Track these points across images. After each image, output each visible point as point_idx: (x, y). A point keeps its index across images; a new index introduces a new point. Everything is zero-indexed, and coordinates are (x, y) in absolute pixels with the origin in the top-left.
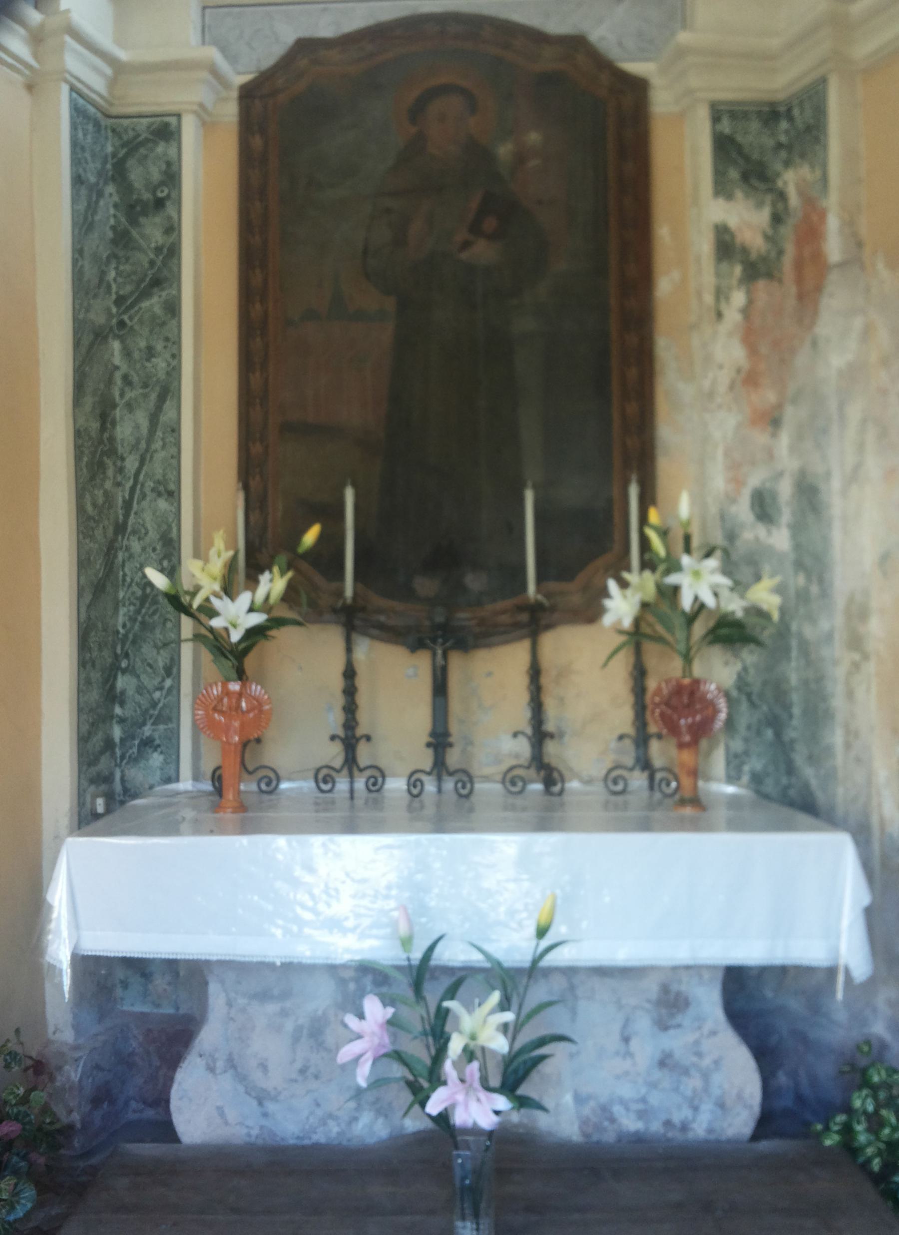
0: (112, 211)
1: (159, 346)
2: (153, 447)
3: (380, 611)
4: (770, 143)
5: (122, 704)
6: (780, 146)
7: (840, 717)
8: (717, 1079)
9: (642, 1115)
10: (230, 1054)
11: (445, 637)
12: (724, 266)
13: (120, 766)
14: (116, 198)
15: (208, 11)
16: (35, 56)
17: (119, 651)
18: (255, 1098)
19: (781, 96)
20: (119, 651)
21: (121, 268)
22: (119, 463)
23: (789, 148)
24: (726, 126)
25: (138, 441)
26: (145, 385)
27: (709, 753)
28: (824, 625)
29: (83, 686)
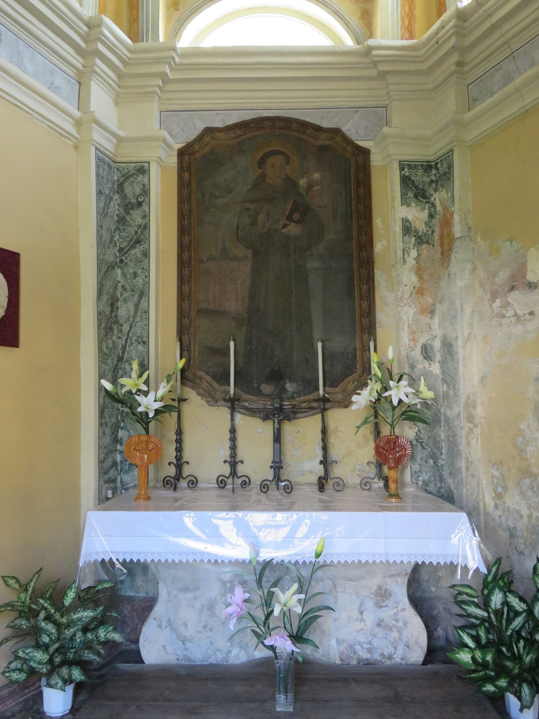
0: (117, 207)
1: (139, 272)
2: (136, 320)
3: (245, 401)
4: (428, 180)
5: (121, 444)
6: (432, 181)
7: (463, 454)
8: (405, 633)
9: (369, 650)
10: (169, 618)
11: (280, 414)
12: (407, 237)
13: (120, 475)
14: (119, 201)
15: (162, 113)
16: (78, 132)
17: (119, 418)
18: (181, 641)
19: (432, 158)
20: (119, 418)
21: (121, 234)
22: (120, 328)
23: (436, 182)
24: (406, 172)
25: (129, 317)
26: (133, 291)
27: (403, 471)
28: (456, 410)
29: (101, 435)
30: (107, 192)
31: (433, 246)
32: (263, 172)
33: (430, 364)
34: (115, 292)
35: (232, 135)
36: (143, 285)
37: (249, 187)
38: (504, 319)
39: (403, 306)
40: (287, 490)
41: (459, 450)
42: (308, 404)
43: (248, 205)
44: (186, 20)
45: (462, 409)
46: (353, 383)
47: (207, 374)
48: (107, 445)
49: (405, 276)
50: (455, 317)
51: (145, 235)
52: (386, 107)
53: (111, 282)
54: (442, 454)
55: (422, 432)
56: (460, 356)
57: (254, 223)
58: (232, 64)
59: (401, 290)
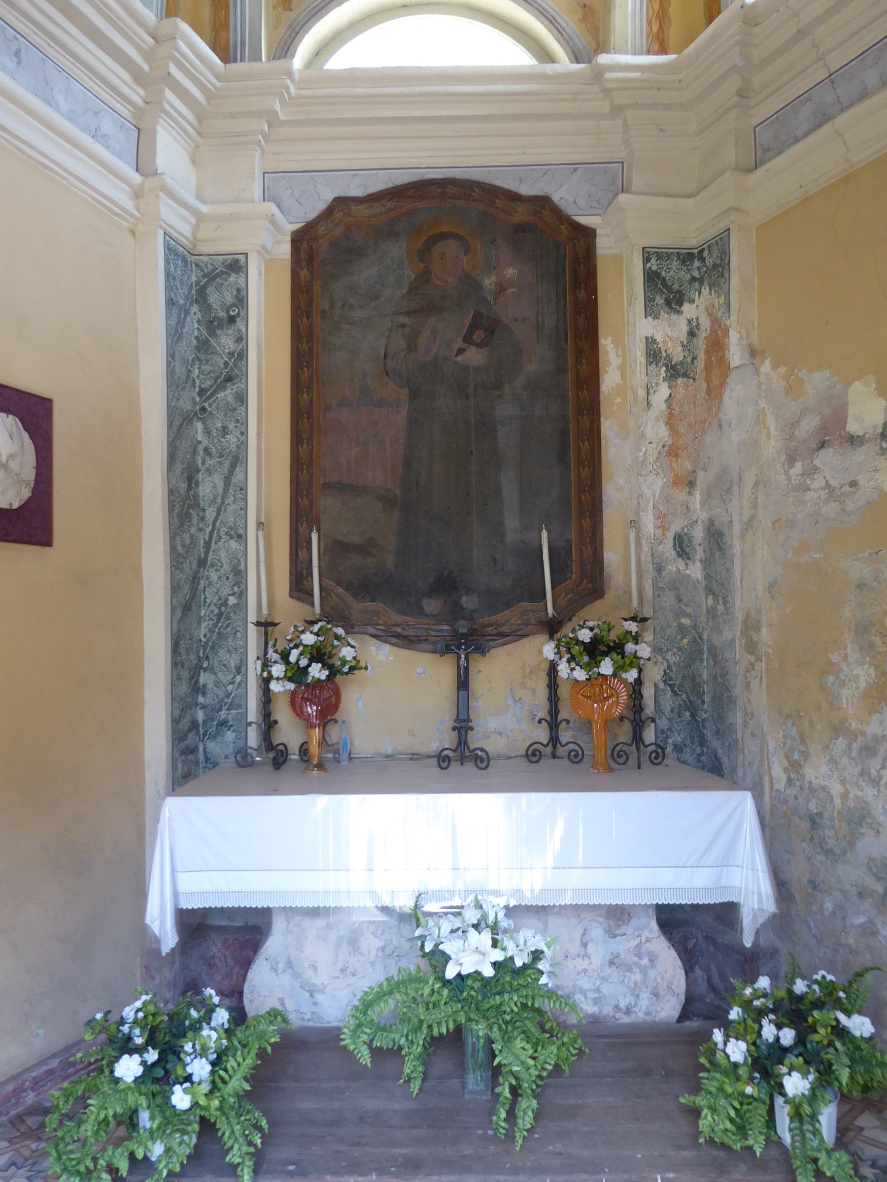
0: (196, 325)
1: (231, 426)
2: (227, 502)
4: (688, 276)
5: (204, 694)
6: (693, 279)
8: (652, 974)
9: (596, 1001)
10: (289, 957)
20: (201, 655)
24: (654, 265)
25: (215, 498)
28: (727, 634)
29: (175, 680)
30: (181, 302)
31: (694, 380)
32: (426, 267)
33: (687, 564)
34: (194, 458)
35: (377, 208)
36: (237, 446)
37: (405, 291)
38: (809, 492)
39: (646, 475)
40: (618, 760)
41: (732, 696)
42: (496, 628)
43: (401, 319)
44: (303, 26)
45: (738, 633)
46: (566, 595)
47: (339, 583)
48: (183, 695)
49: (649, 427)
50: (728, 491)
51: (240, 369)
52: (622, 163)
53: (189, 443)
54: (703, 702)
55: (674, 669)
56: (737, 550)
57: (412, 346)
58: (373, 96)
59: (644, 449)
